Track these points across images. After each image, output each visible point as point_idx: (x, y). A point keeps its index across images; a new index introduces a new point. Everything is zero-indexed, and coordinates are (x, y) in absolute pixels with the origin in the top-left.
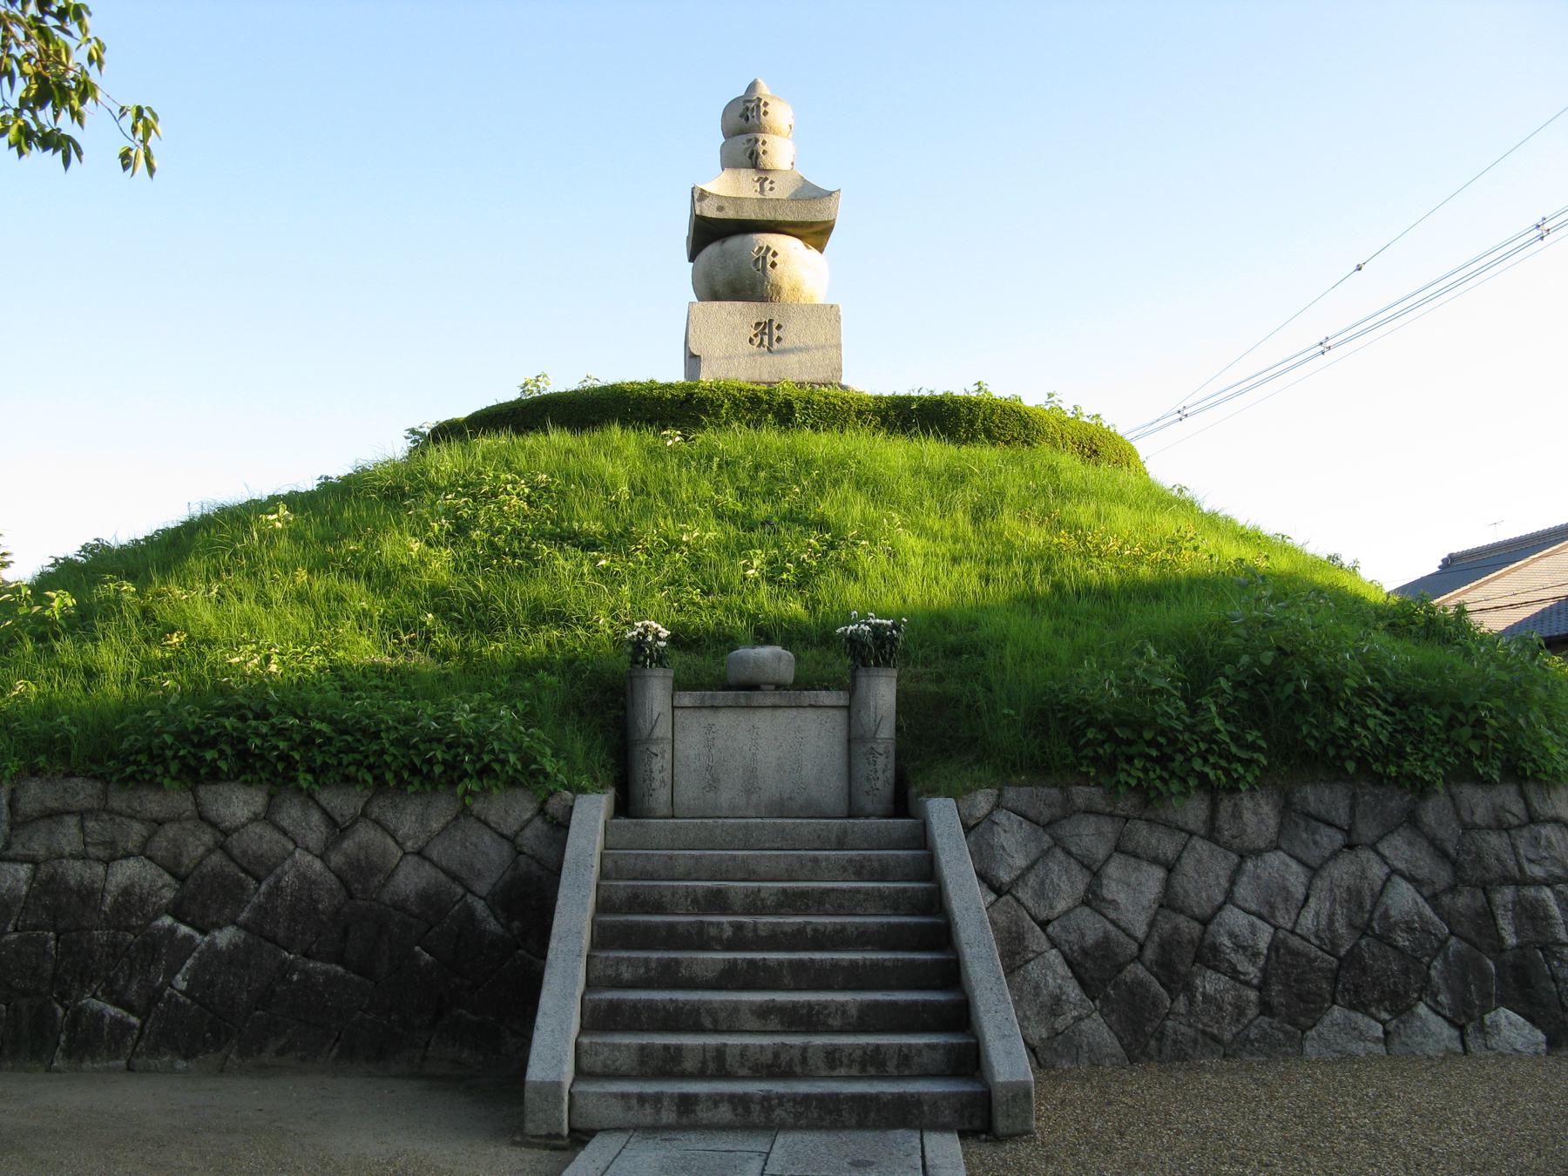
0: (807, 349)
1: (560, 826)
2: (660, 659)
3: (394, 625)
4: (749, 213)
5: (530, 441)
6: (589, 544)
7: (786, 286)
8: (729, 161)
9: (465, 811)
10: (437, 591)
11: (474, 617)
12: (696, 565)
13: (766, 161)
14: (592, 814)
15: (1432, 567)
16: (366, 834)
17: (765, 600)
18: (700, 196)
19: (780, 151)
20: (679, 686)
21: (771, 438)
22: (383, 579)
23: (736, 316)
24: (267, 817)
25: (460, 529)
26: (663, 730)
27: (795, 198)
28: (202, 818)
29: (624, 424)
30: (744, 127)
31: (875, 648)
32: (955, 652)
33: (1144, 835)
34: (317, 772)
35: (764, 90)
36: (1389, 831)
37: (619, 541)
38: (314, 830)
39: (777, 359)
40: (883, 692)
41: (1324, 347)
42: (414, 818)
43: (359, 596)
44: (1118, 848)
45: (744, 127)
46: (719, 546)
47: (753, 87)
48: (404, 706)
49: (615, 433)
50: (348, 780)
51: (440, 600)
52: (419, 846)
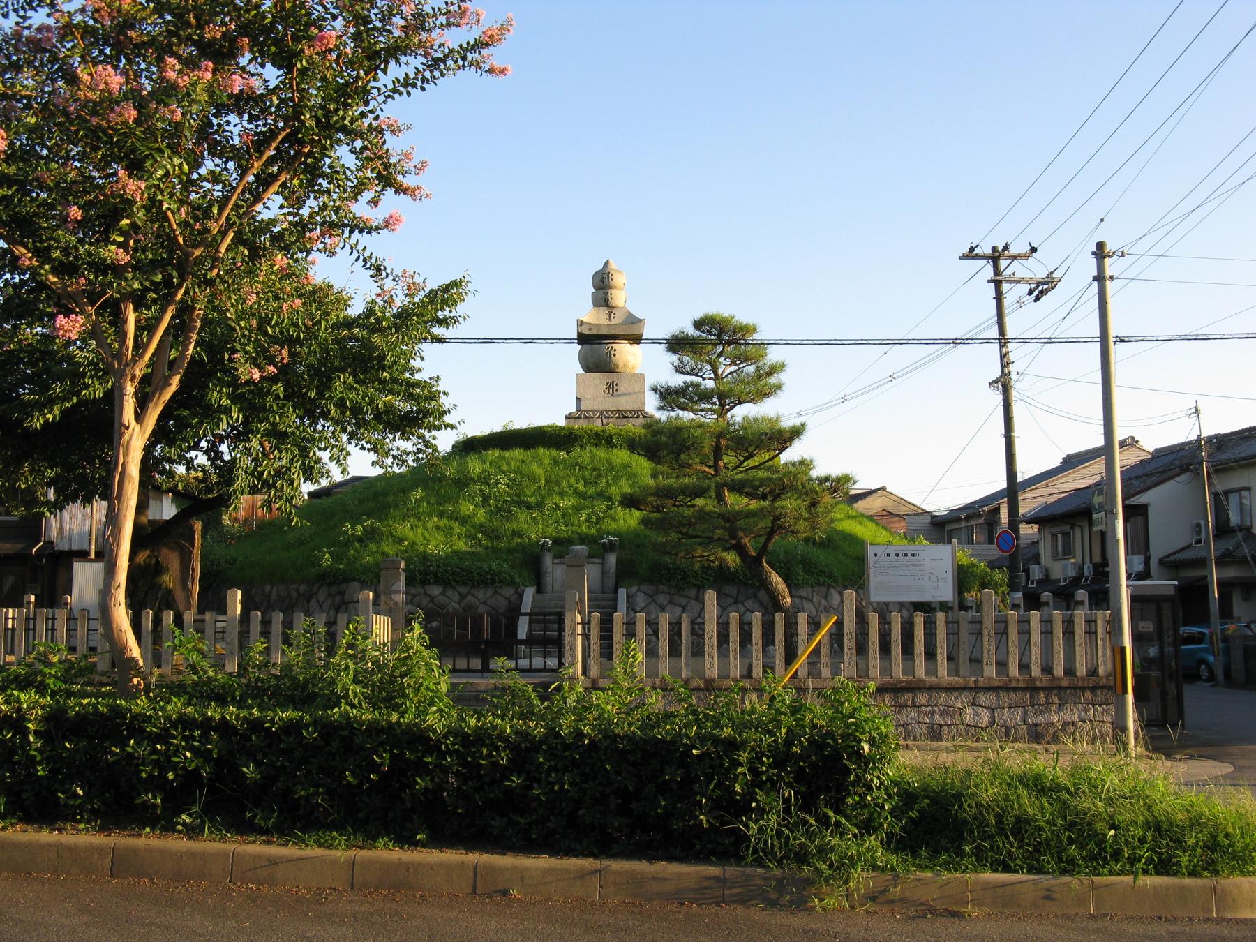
0: (629, 394)
1: (521, 596)
2: (549, 550)
3: (470, 537)
4: (604, 331)
5: (507, 454)
6: (529, 507)
7: (621, 364)
8: (597, 304)
9: (496, 592)
10: (481, 526)
11: (493, 534)
12: (564, 516)
13: (612, 303)
14: (529, 593)
15: (1056, 462)
16: (469, 598)
17: (584, 529)
18: (581, 323)
19: (619, 298)
20: (555, 557)
21: (601, 453)
22: (464, 521)
23: (598, 379)
24: (443, 594)
25: (486, 499)
26: (550, 570)
27: (625, 323)
28: (426, 594)
29: (544, 447)
30: (602, 283)
31: (610, 547)
32: (638, 546)
33: (677, 599)
34: (457, 582)
35: (613, 265)
36: (748, 598)
37: (539, 506)
38: (456, 597)
39: (615, 399)
40: (612, 559)
41: (892, 378)
42: (482, 594)
43: (457, 528)
44: (670, 602)
45: (602, 283)
46: (573, 507)
47: (607, 264)
48: (478, 564)
49: (541, 450)
50: (465, 584)
51: (482, 528)
52: (484, 600)
